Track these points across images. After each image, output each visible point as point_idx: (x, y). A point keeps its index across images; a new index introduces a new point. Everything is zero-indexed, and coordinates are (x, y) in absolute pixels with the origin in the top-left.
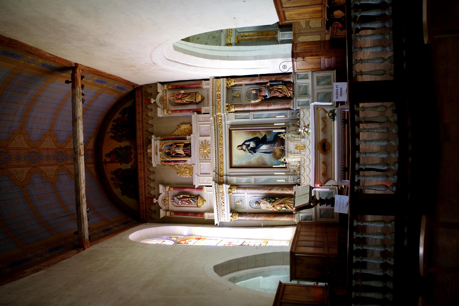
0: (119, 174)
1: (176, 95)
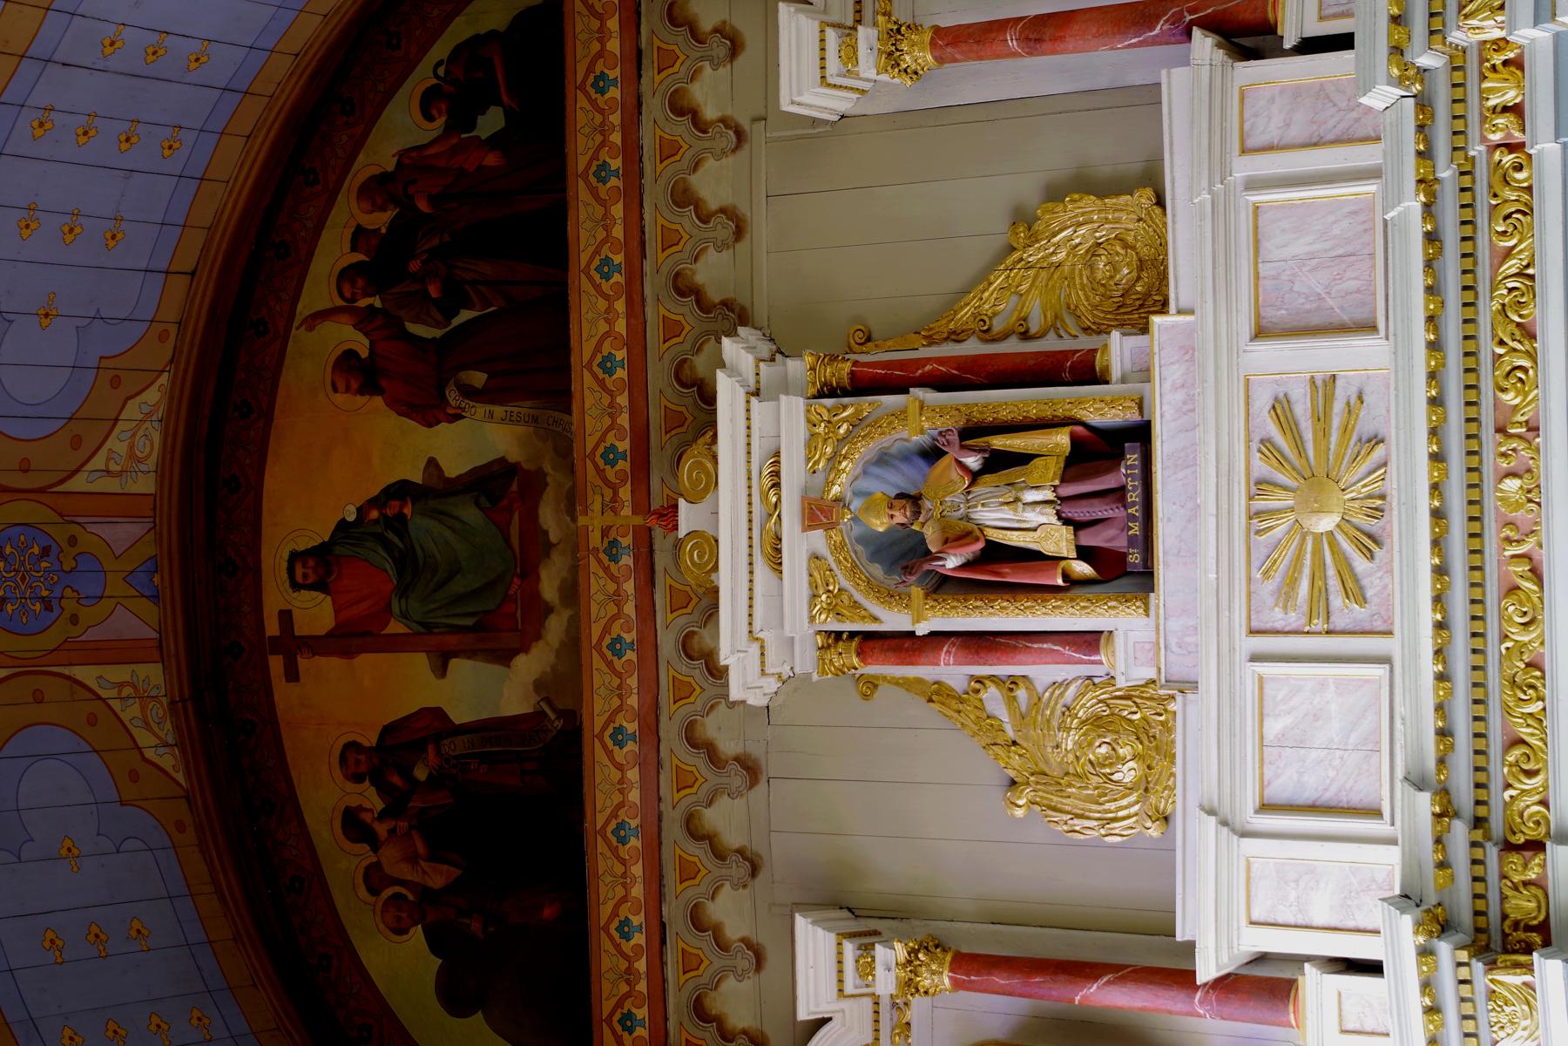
0: (421, 774)
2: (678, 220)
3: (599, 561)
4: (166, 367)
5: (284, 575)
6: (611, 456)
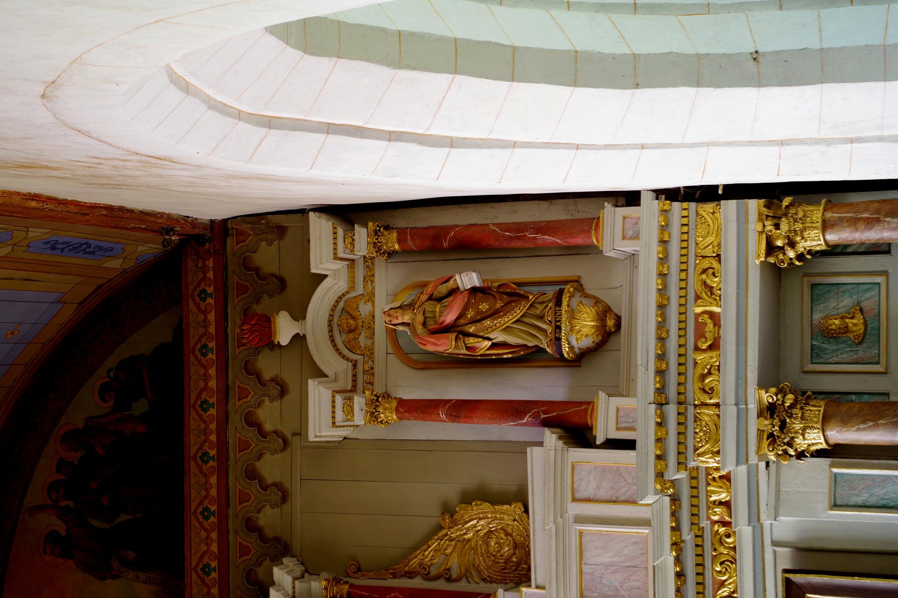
1: (430, 298)
6: (203, 295)
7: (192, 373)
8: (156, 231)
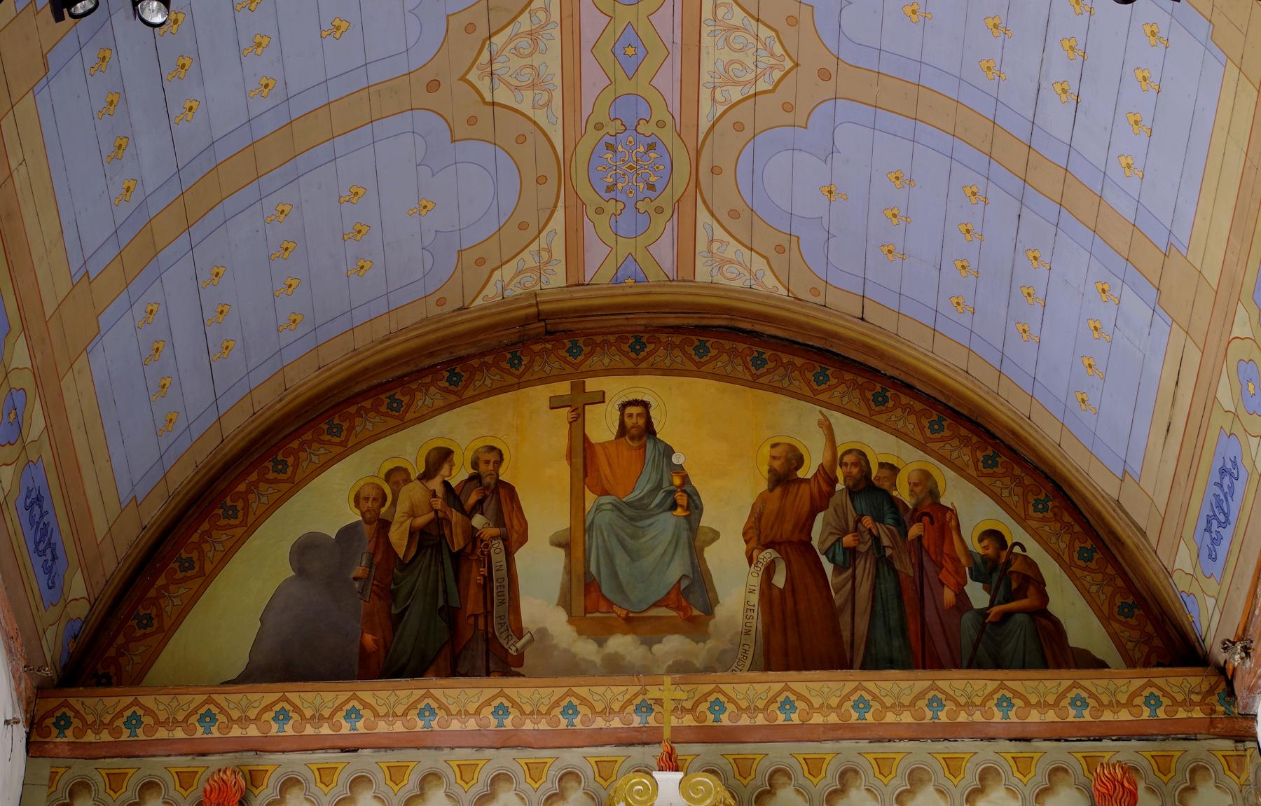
0: (478, 521)
2: (899, 774)
3: (636, 695)
4: (792, 293)
5: (631, 397)
7: (1047, 683)
8: (1245, 630)
